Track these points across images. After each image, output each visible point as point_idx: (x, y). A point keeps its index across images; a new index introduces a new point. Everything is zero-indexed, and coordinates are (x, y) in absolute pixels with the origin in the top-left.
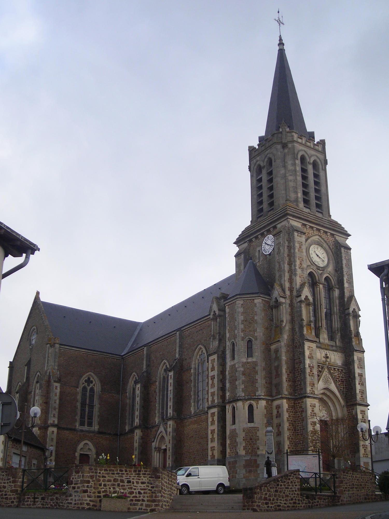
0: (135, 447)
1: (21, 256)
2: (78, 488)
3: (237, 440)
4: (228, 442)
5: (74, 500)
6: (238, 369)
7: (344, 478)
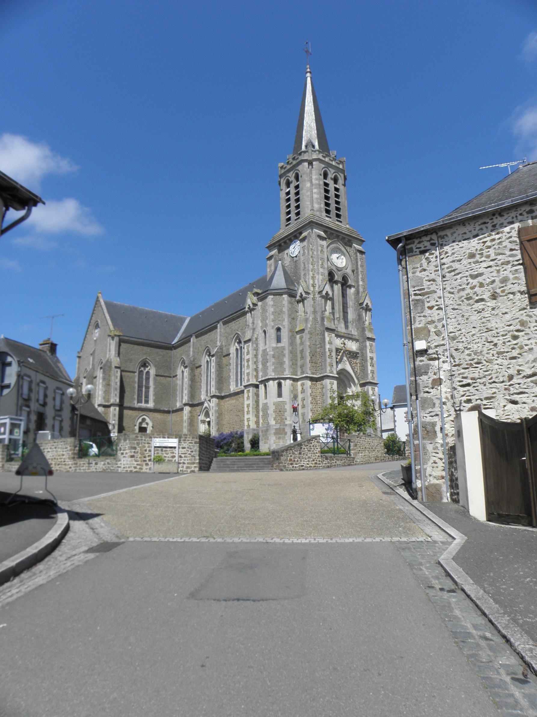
0: (184, 420)
1: (24, 208)
2: (126, 453)
3: (268, 412)
4: (261, 414)
5: (123, 464)
6: (269, 353)
7: (358, 442)
